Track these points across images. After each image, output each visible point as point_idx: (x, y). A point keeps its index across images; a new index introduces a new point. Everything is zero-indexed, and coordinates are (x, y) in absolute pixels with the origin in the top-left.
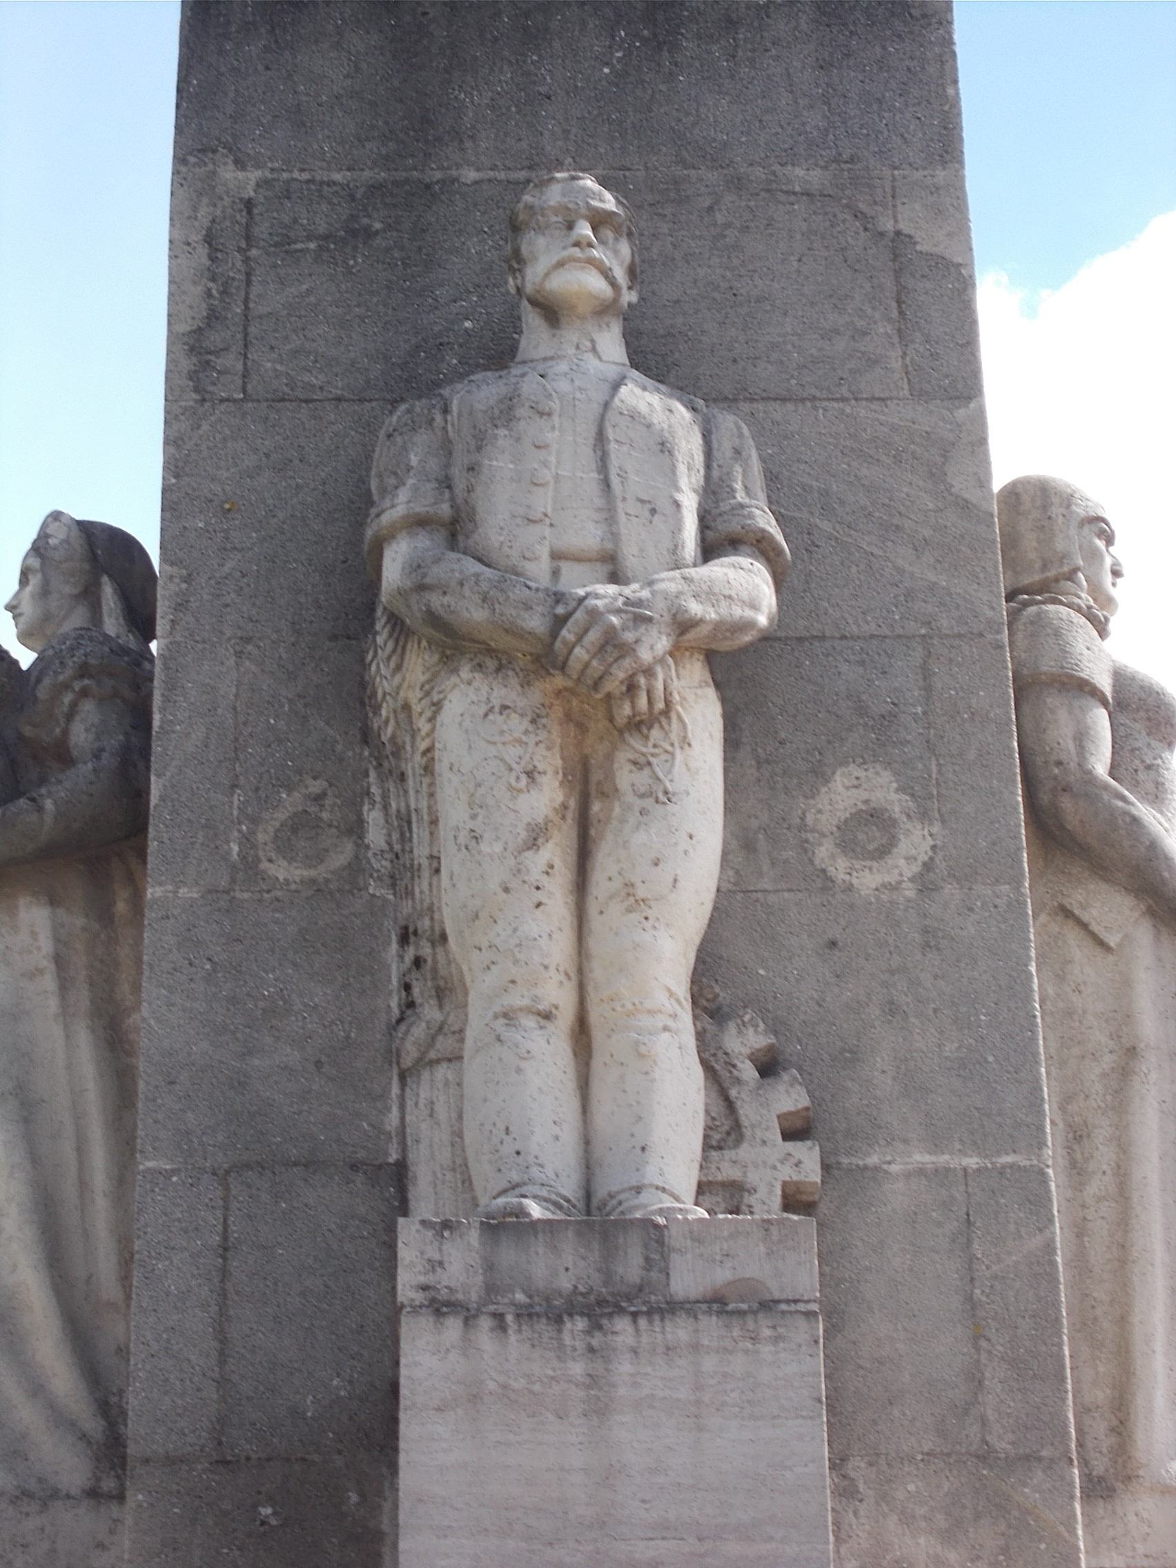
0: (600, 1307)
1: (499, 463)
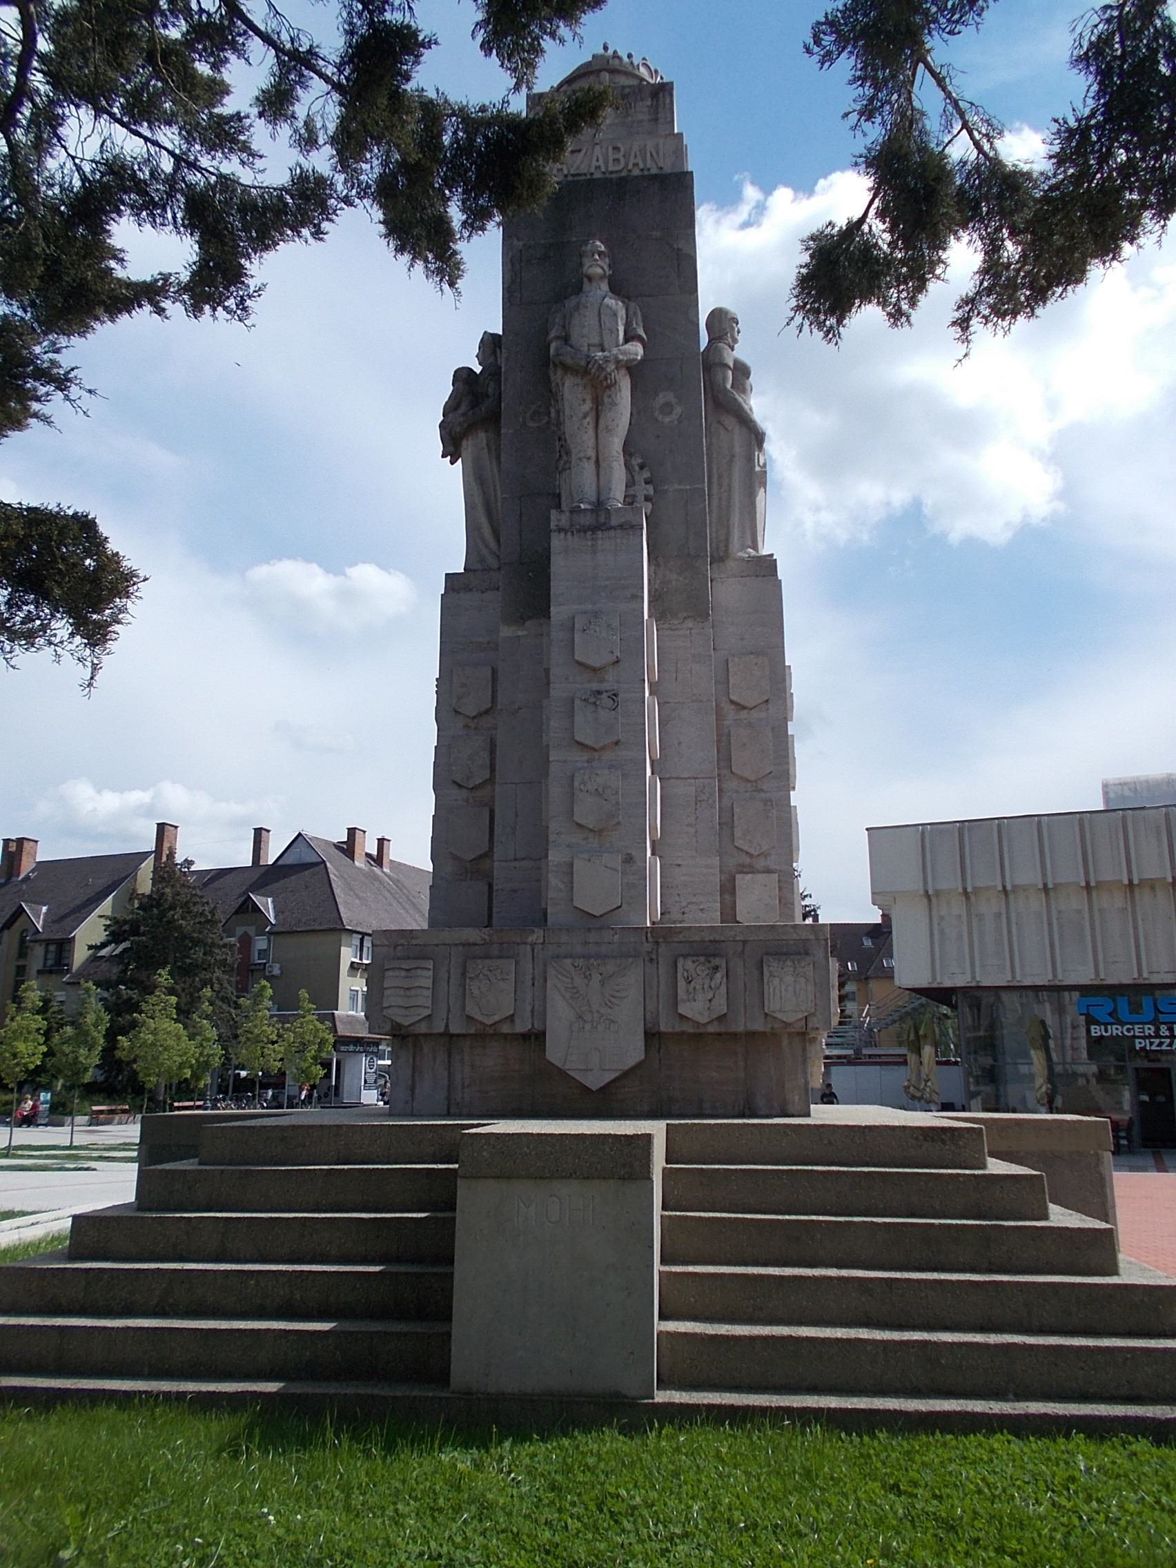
0: (594, 529)
1: (576, 321)
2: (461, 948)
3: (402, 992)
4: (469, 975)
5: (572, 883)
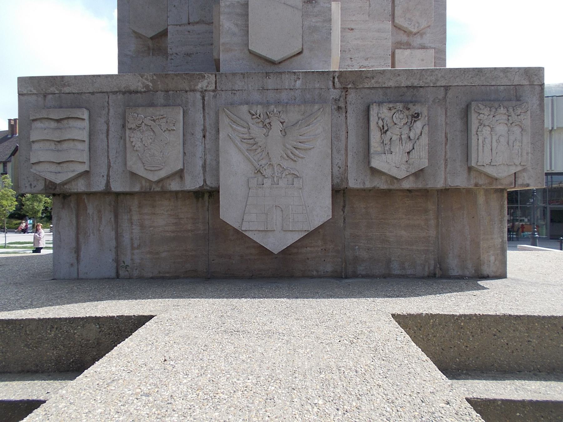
2: (120, 96)
3: (53, 146)
4: (129, 126)
5: (247, 26)
